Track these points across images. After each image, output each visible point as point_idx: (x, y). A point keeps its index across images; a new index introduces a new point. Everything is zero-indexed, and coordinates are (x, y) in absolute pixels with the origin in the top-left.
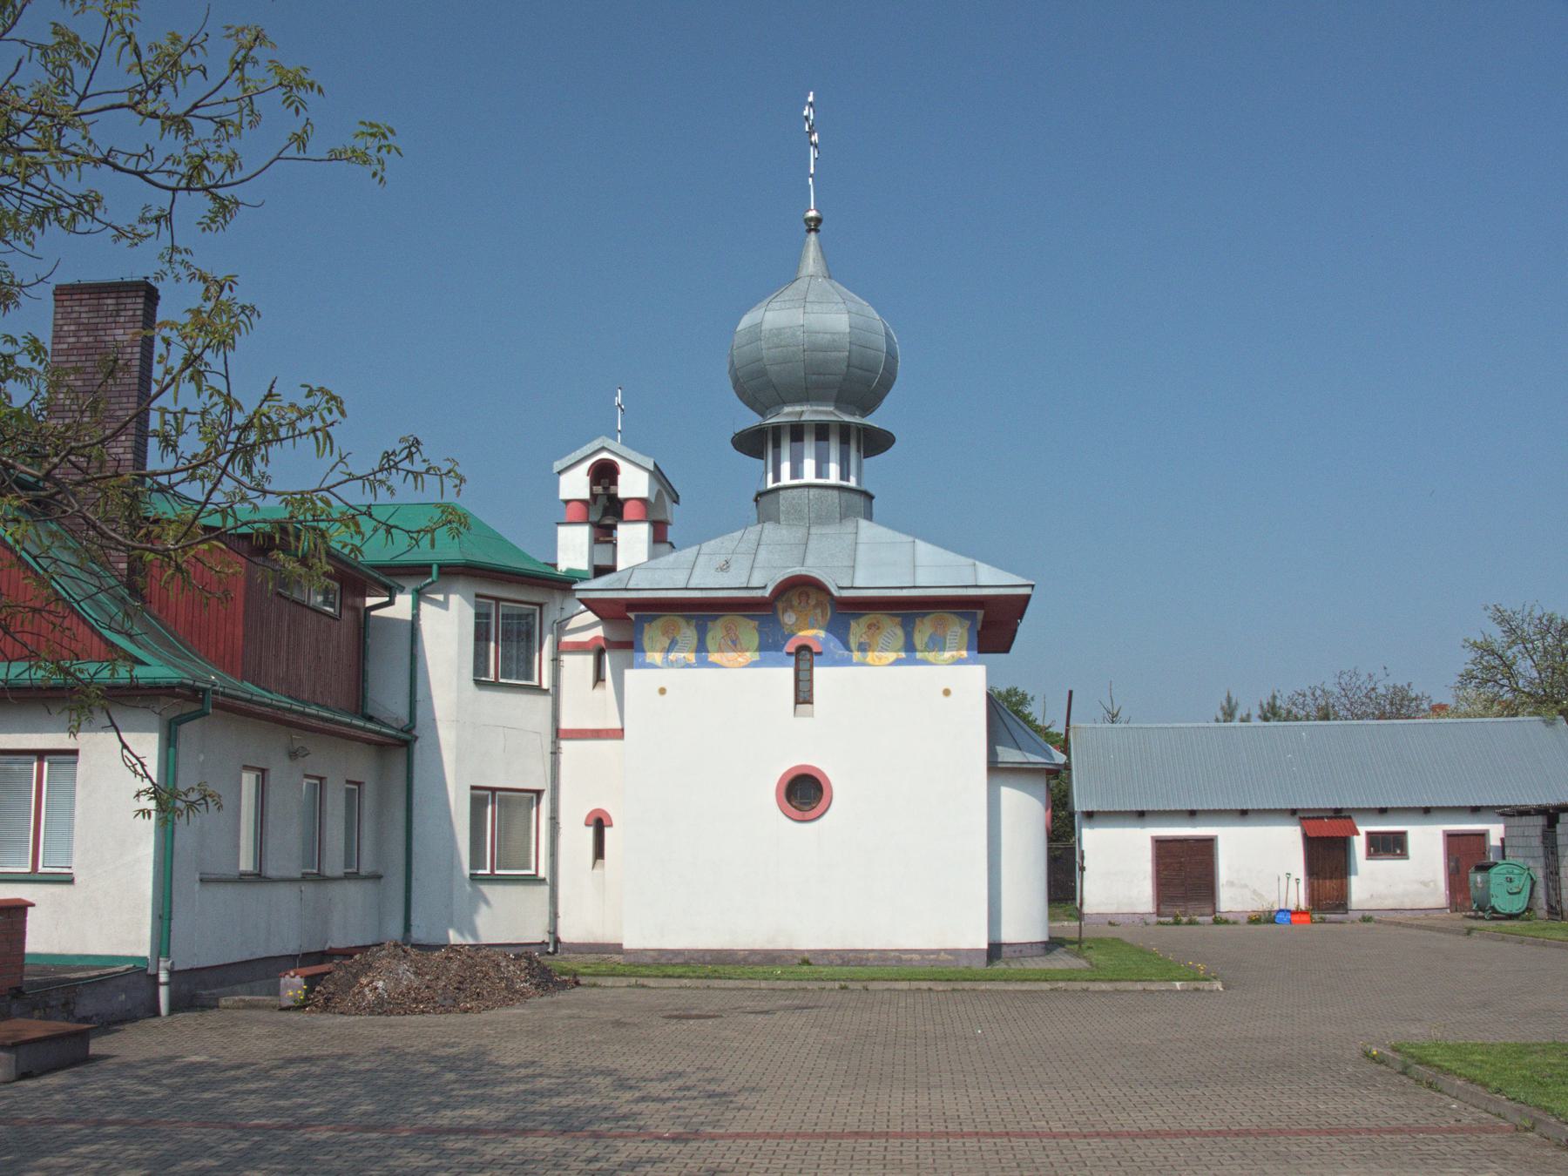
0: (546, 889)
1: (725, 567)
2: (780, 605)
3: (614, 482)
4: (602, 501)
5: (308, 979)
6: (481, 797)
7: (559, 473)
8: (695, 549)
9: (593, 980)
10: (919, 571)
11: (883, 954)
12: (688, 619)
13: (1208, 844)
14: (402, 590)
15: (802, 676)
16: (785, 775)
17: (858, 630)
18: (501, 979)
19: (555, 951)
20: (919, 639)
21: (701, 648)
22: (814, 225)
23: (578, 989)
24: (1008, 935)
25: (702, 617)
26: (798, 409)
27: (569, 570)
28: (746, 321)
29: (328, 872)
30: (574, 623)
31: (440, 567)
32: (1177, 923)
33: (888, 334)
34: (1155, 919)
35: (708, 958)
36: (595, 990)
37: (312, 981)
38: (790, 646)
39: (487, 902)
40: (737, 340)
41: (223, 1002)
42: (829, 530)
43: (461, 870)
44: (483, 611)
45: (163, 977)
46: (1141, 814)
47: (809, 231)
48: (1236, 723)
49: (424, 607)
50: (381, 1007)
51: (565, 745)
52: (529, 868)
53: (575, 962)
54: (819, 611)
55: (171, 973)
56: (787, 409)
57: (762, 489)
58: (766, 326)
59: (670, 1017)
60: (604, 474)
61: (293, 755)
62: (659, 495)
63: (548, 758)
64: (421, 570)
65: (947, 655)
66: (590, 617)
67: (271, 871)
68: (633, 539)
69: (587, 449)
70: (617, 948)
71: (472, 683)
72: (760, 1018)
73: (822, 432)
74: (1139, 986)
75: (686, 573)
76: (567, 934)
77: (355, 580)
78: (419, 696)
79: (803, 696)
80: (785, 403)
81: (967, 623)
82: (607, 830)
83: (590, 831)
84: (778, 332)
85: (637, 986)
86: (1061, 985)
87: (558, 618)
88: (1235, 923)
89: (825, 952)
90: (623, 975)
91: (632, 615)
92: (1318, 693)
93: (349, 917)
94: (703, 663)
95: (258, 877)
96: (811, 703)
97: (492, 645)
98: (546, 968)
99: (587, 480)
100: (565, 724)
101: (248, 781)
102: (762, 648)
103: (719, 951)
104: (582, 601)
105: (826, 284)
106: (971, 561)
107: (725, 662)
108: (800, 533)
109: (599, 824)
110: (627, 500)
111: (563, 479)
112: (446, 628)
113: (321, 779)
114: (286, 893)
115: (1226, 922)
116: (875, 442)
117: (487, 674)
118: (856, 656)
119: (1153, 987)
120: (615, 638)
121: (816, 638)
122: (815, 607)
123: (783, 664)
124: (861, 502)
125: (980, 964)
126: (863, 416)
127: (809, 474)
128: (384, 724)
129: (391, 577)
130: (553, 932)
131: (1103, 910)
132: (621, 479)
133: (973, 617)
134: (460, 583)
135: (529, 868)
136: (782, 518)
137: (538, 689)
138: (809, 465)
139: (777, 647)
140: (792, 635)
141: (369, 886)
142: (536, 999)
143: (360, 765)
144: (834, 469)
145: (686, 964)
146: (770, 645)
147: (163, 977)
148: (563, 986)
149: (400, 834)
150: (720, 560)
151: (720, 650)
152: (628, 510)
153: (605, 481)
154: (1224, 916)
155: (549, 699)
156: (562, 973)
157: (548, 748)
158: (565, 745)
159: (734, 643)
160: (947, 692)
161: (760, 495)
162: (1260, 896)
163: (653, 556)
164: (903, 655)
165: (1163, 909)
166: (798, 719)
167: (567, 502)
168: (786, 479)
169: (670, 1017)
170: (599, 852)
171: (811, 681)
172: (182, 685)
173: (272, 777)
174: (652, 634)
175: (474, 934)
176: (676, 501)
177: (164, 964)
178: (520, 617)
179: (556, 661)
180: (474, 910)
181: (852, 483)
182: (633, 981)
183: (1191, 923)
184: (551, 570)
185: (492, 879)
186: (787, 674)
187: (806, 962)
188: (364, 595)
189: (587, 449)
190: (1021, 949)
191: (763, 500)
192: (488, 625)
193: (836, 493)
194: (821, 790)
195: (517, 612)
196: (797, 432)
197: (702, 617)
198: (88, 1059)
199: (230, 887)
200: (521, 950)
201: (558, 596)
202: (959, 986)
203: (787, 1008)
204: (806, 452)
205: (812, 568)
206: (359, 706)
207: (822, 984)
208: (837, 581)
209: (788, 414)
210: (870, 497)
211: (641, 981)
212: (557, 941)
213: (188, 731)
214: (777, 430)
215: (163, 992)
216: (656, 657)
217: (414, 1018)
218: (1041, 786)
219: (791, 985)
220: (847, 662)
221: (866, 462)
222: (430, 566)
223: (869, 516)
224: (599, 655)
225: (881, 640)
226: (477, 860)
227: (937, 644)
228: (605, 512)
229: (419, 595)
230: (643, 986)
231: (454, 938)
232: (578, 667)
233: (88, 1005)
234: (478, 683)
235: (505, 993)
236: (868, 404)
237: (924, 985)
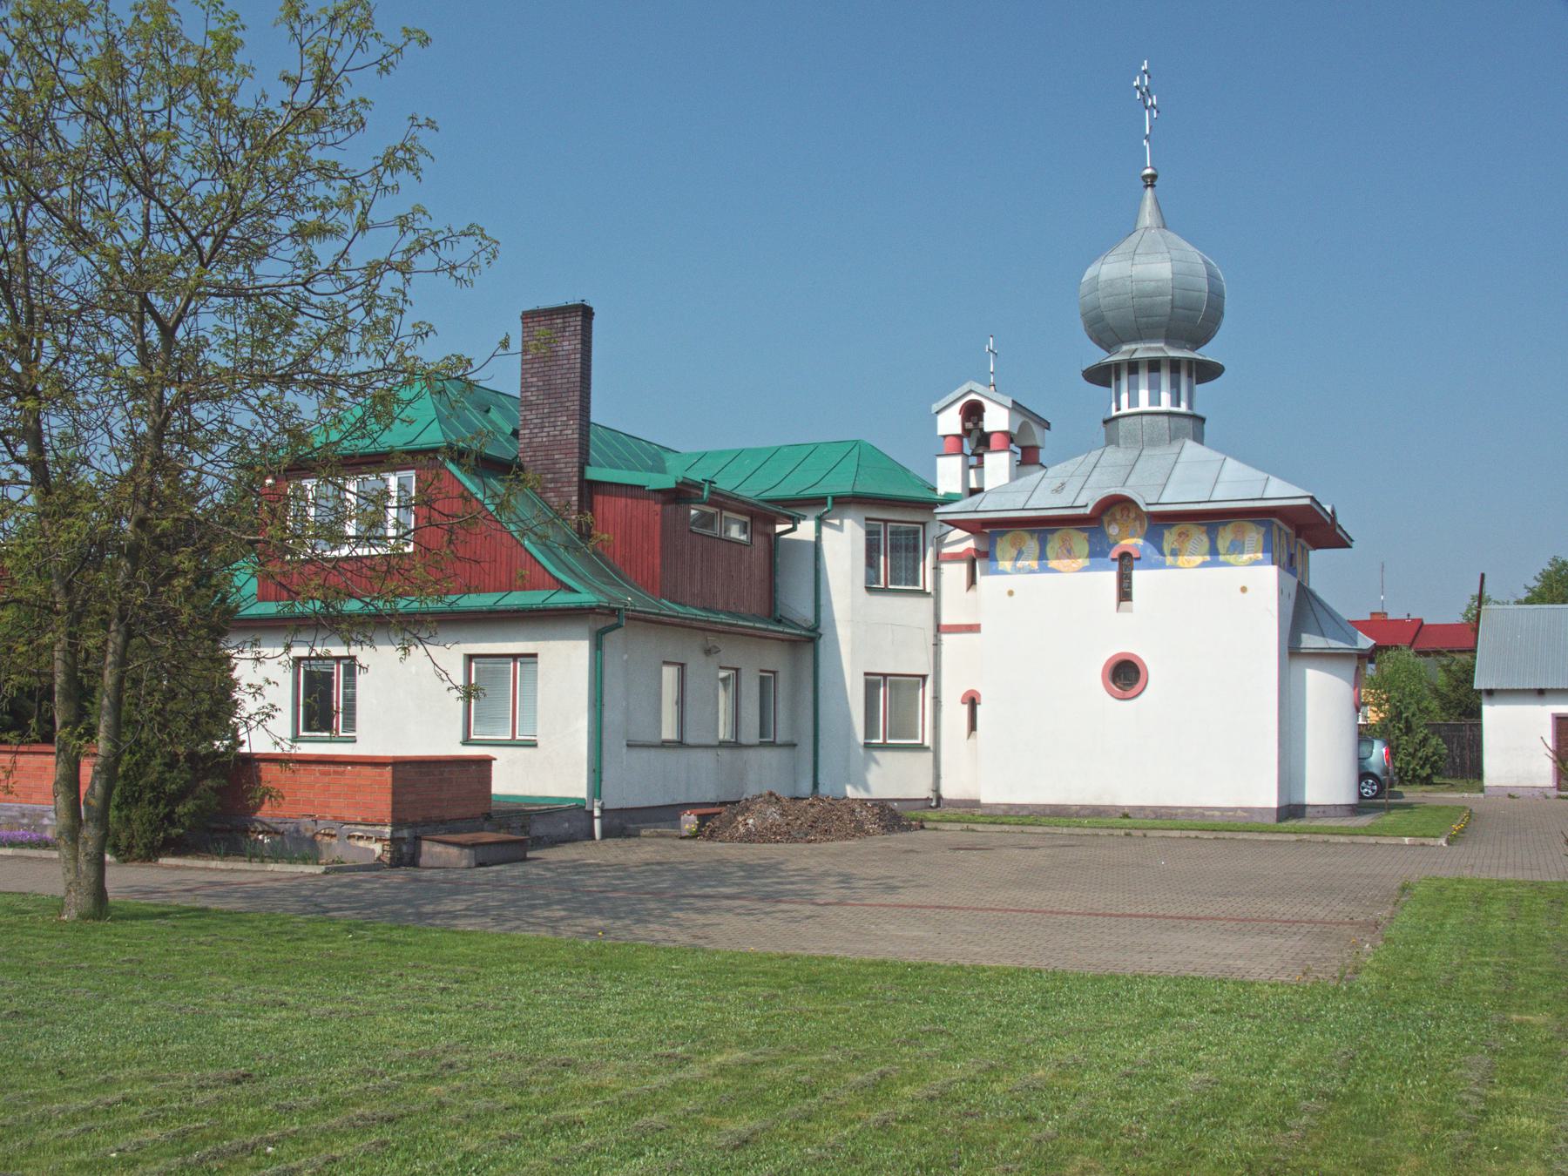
0: (929, 756)
2: (1106, 519)
3: (981, 419)
5: (699, 816)
11: (1189, 811)
12: (1032, 533)
14: (805, 518)
17: (1170, 538)
19: (938, 805)
20: (1222, 544)
21: (1042, 556)
23: (921, 832)
24: (1314, 794)
25: (1041, 530)
26: (1134, 346)
27: (947, 494)
28: (1090, 273)
29: (743, 740)
31: (834, 498)
34: (1555, 792)
37: (703, 819)
38: (1114, 553)
39: (877, 762)
41: (643, 832)
42: (1157, 451)
43: (855, 740)
45: (597, 813)
46: (1541, 692)
49: (825, 531)
50: (749, 838)
51: (945, 637)
52: (916, 737)
55: (602, 810)
56: (1125, 348)
58: (1102, 278)
60: (973, 412)
61: (708, 652)
63: (931, 649)
64: (819, 501)
65: (1246, 557)
67: (689, 740)
69: (958, 393)
70: (975, 804)
73: (1154, 366)
76: (948, 792)
77: (765, 515)
78: (823, 601)
79: (1125, 594)
80: (1123, 342)
83: (965, 708)
84: (1111, 283)
87: (938, 533)
89: (1142, 808)
93: (765, 772)
94: (1044, 569)
95: (680, 744)
99: (958, 418)
100: (945, 621)
101: (669, 675)
102: (1091, 555)
103: (1057, 806)
109: (972, 702)
111: (940, 418)
112: (842, 546)
113: (737, 670)
114: (705, 759)
116: (1207, 372)
118: (1169, 560)
122: (1135, 519)
123: (1107, 568)
124: (1195, 425)
125: (1271, 820)
126: (1193, 349)
128: (799, 626)
129: (793, 508)
130: (937, 790)
131: (1503, 783)
132: (986, 415)
134: (852, 511)
135: (916, 737)
137: (923, 593)
138: (1144, 394)
139: (1104, 554)
141: (784, 753)
143: (774, 658)
144: (1165, 397)
146: (1097, 553)
147: (597, 813)
148: (909, 828)
149: (809, 712)
150: (1057, 483)
151: (1058, 558)
152: (994, 441)
153: (975, 419)
155: (931, 601)
157: (931, 640)
158: (945, 637)
159: (1069, 551)
163: (1014, 477)
164: (1208, 558)
166: (1121, 614)
167: (945, 436)
168: (1125, 410)
170: (973, 726)
172: (599, 607)
173: (689, 671)
174: (1004, 546)
175: (867, 789)
176: (1047, 426)
177: (597, 803)
178: (907, 533)
179: (936, 569)
180: (866, 767)
181: (1183, 408)
185: (884, 747)
186: (1110, 578)
187: (1126, 816)
188: (774, 522)
189: (958, 393)
190: (1325, 810)
193: (1166, 418)
194: (1138, 672)
195: (901, 532)
196: (1133, 367)
197: (1041, 530)
198: (525, 859)
199: (653, 752)
202: (1221, 835)
206: (773, 612)
210: (1203, 420)
211: (971, 826)
212: (939, 798)
213: (612, 639)
214: (1117, 367)
215: (597, 823)
218: (1349, 668)
220: (1161, 565)
221: (1199, 388)
223: (1199, 438)
225: (1189, 545)
226: (870, 729)
227: (1236, 548)
229: (820, 521)
231: (851, 792)
232: (955, 573)
233: (539, 829)
234: (869, 589)
236: (1200, 337)
237: (1193, 834)
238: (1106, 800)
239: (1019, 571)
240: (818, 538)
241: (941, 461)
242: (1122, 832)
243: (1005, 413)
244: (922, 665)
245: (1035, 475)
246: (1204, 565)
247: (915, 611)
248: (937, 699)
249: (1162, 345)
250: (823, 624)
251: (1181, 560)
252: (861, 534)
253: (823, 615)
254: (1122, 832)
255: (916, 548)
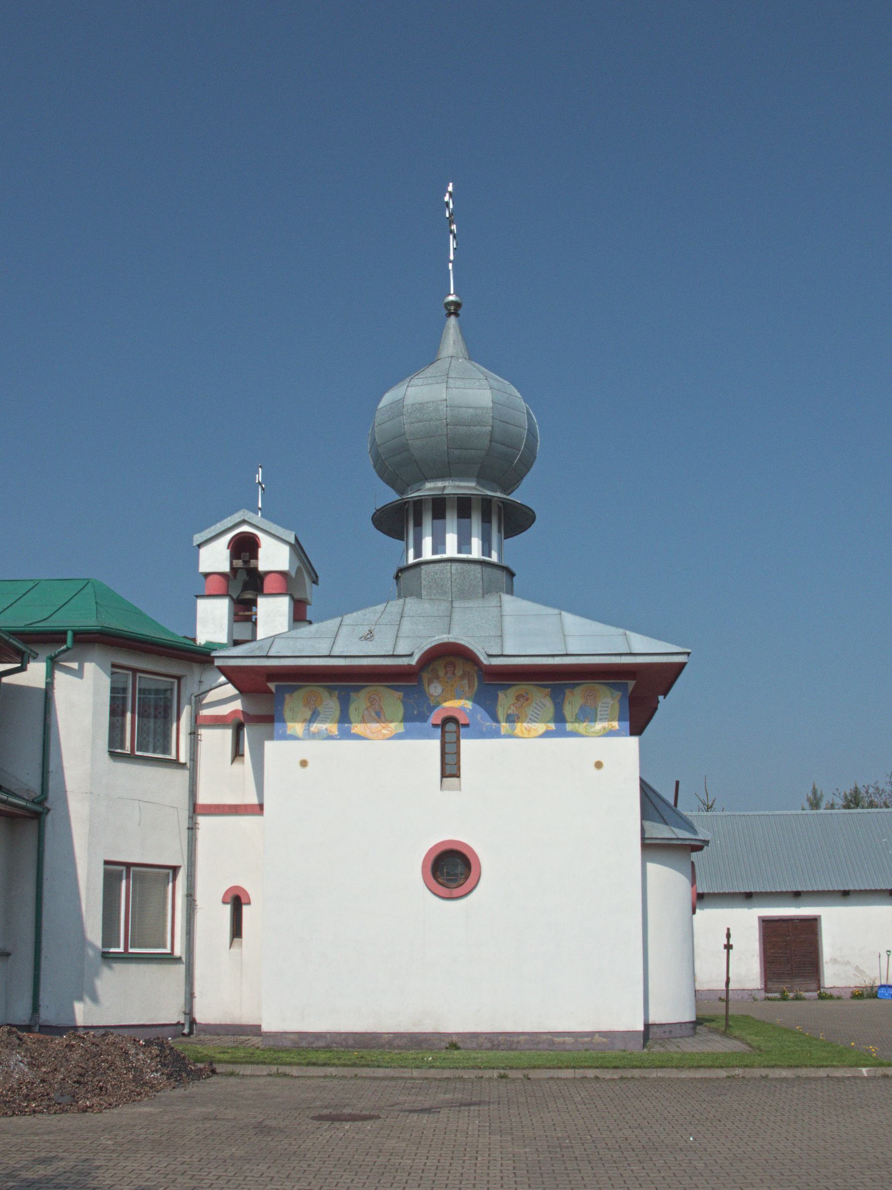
0: (181, 968)
1: (369, 636)
2: (425, 676)
3: (255, 556)
4: (243, 576)
6: (114, 873)
7: (199, 546)
8: (337, 620)
9: (230, 1068)
10: (570, 640)
11: (534, 1038)
12: (330, 689)
13: (812, 923)
14: (35, 658)
15: (449, 748)
16: (431, 850)
17: (505, 701)
18: (129, 1069)
19: (191, 1033)
20: (569, 710)
21: (344, 718)
22: (454, 309)
23: (214, 1079)
26: (440, 484)
28: (387, 399)
30: (211, 697)
31: (76, 633)
32: (784, 998)
33: (528, 414)
34: (763, 994)
35: (351, 1042)
36: (232, 1080)
38: (436, 717)
40: (379, 417)
44: (120, 685)
46: (749, 896)
47: (449, 314)
48: (821, 811)
49: (59, 676)
51: (203, 821)
52: (164, 947)
53: (209, 1048)
54: (466, 681)
56: (429, 485)
57: (403, 565)
58: (408, 401)
59: (321, 1118)
60: (244, 547)
62: (299, 570)
63: (185, 834)
64: (54, 637)
65: (599, 726)
66: (230, 690)
68: (272, 613)
70: (256, 1030)
71: (107, 755)
72: (425, 1118)
73: (464, 507)
74: (822, 1073)
75: (329, 642)
78: (52, 767)
79: (450, 768)
80: (427, 479)
81: (618, 694)
82: (245, 909)
83: (228, 909)
84: (421, 407)
85: (278, 1075)
86: (738, 1072)
88: (839, 998)
89: (475, 1035)
90: (264, 1063)
91: (272, 686)
92: (871, 790)
94: (346, 735)
96: (458, 776)
97: (129, 715)
98: (181, 1055)
99: (227, 553)
100: (203, 799)
102: (406, 719)
104: (223, 670)
105: (468, 365)
106: (621, 631)
107: (369, 735)
108: (445, 605)
109: (237, 901)
110: (268, 573)
111: (203, 551)
112: (81, 697)
115: (831, 997)
117: (122, 746)
118: (504, 726)
119: (839, 1073)
120: (252, 711)
121: (462, 709)
122: (462, 678)
123: (428, 736)
124: (502, 578)
125: (636, 1047)
127: (451, 549)
130: (189, 1012)
132: (261, 552)
133: (622, 688)
134: (97, 651)
135: (164, 947)
136: (424, 592)
137: (176, 763)
138: (451, 540)
139: (423, 718)
140: (438, 704)
142: (169, 1093)
144: (476, 543)
145: (328, 1048)
146: (415, 716)
148: (198, 1075)
150: (365, 630)
151: (363, 721)
152: (269, 584)
154: (828, 992)
155: (186, 773)
156: (198, 1060)
157: (185, 823)
158: (203, 821)
159: (379, 717)
160: (599, 765)
161: (401, 570)
162: (862, 972)
163: (291, 628)
164: (552, 726)
165: (770, 985)
166: (446, 793)
167: (207, 575)
168: (427, 554)
169: (321, 1118)
170: (237, 931)
171: (458, 753)
174: (293, 703)
176: (315, 581)
178: (157, 691)
179: (194, 734)
181: (494, 558)
182: (274, 1069)
183: (797, 998)
184: (192, 643)
185: (126, 958)
186: (434, 746)
190: (670, 1030)
191: (404, 576)
192: (124, 699)
193: (478, 568)
195: (154, 683)
196: (438, 507)
197: (344, 686)
200: (152, 1034)
201: (196, 668)
202: (628, 1073)
203: (450, 1104)
204: (448, 528)
205: (458, 636)
207: (480, 1073)
208: (484, 650)
209: (430, 489)
210: (512, 574)
211: (282, 1069)
212: (193, 1022)
214: (418, 504)
216: (297, 728)
217: (24, 1119)
219: (447, 1073)
220: (495, 734)
222: (65, 633)
223: (510, 592)
224: (238, 729)
226: (109, 936)
227: (588, 715)
228: (245, 585)
229: (53, 664)
230: (285, 1075)
232: (216, 742)
234: (113, 754)
235: (131, 1086)
236: (510, 482)
237: (591, 1073)
238: (428, 1027)
239: (313, 736)
240: (50, 685)
241: (202, 604)
242: (495, 1074)
243: (285, 550)
244: (173, 856)
245: (305, 630)
246: (547, 734)
247: (162, 786)
248: (190, 897)
249: (473, 484)
250: (51, 794)
251: (520, 727)
252: (106, 682)
253: (52, 784)
254: (495, 1074)
255: (167, 709)
